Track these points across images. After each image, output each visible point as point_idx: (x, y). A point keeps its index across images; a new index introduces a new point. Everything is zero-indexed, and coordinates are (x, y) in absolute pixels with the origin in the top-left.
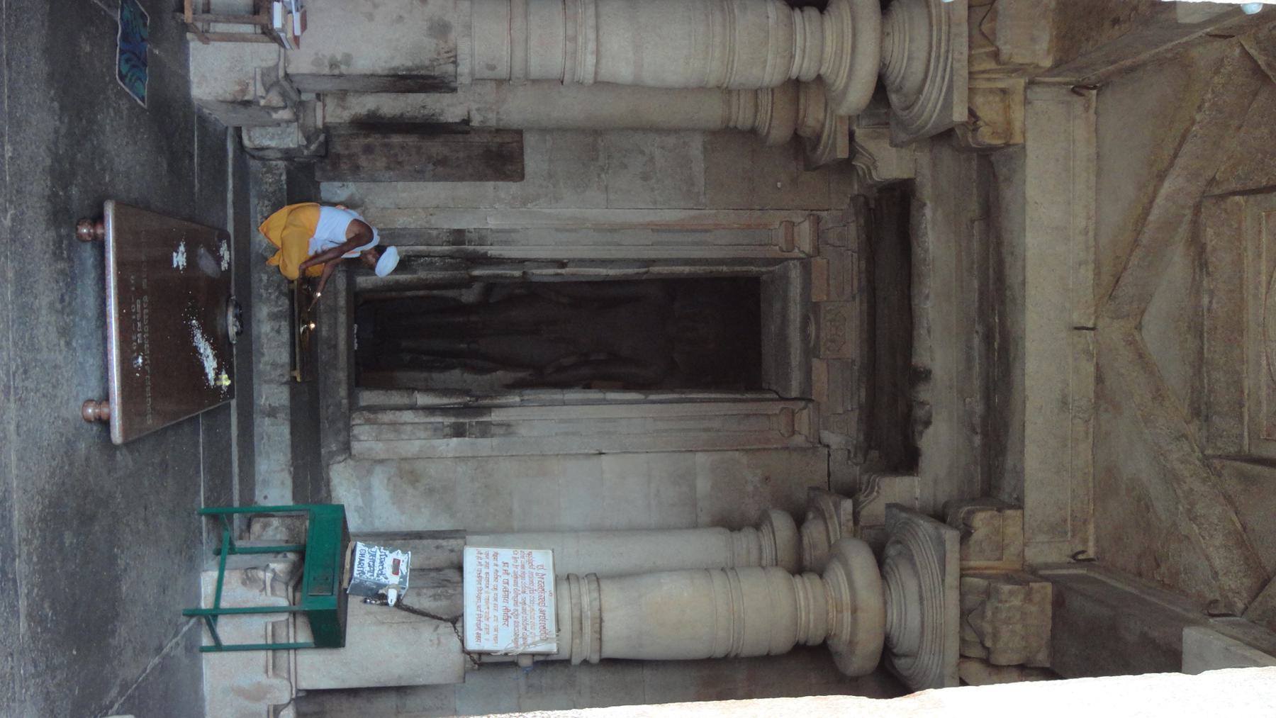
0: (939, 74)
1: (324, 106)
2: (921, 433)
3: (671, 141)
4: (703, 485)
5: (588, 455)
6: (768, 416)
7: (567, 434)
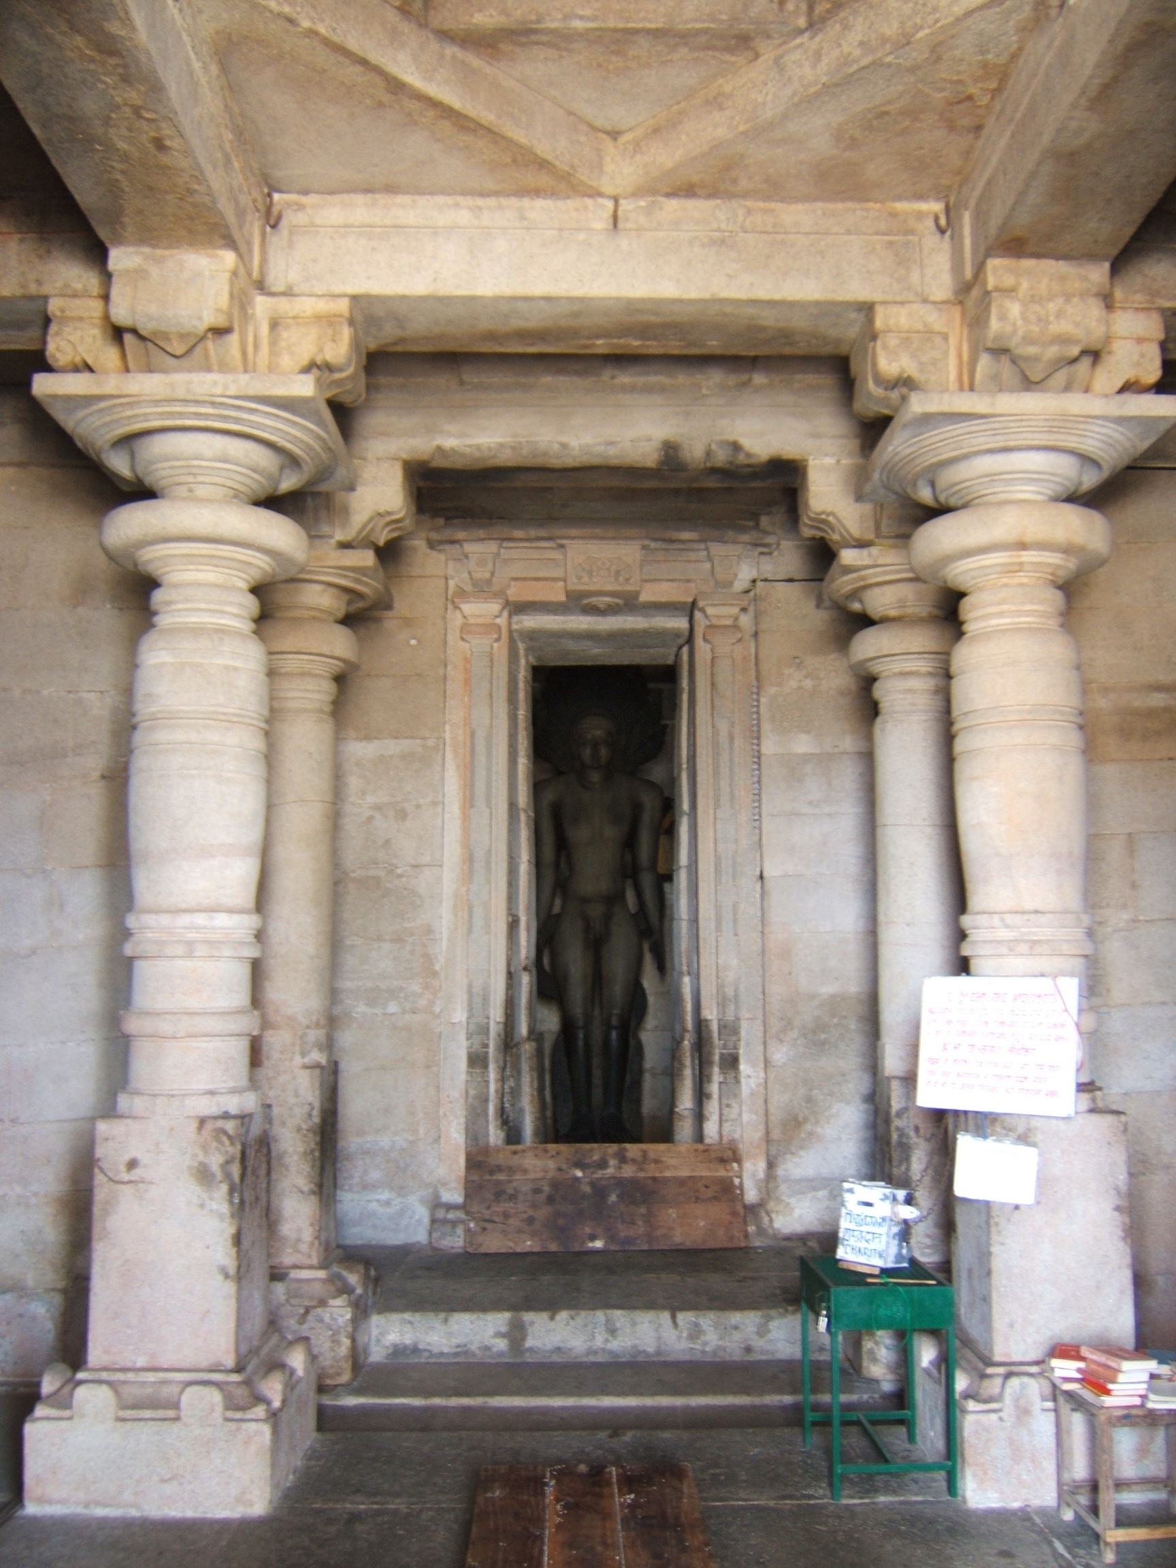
0: (245, 416)
1: (296, 1267)
2: (748, 455)
3: (354, 783)
4: (803, 744)
5: (763, 894)
6: (713, 659)
7: (735, 921)
